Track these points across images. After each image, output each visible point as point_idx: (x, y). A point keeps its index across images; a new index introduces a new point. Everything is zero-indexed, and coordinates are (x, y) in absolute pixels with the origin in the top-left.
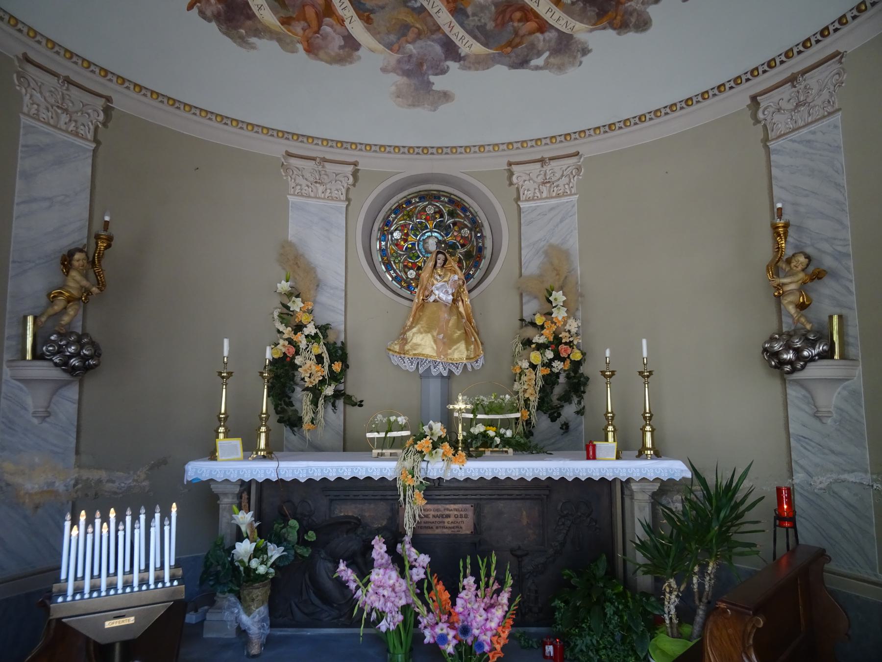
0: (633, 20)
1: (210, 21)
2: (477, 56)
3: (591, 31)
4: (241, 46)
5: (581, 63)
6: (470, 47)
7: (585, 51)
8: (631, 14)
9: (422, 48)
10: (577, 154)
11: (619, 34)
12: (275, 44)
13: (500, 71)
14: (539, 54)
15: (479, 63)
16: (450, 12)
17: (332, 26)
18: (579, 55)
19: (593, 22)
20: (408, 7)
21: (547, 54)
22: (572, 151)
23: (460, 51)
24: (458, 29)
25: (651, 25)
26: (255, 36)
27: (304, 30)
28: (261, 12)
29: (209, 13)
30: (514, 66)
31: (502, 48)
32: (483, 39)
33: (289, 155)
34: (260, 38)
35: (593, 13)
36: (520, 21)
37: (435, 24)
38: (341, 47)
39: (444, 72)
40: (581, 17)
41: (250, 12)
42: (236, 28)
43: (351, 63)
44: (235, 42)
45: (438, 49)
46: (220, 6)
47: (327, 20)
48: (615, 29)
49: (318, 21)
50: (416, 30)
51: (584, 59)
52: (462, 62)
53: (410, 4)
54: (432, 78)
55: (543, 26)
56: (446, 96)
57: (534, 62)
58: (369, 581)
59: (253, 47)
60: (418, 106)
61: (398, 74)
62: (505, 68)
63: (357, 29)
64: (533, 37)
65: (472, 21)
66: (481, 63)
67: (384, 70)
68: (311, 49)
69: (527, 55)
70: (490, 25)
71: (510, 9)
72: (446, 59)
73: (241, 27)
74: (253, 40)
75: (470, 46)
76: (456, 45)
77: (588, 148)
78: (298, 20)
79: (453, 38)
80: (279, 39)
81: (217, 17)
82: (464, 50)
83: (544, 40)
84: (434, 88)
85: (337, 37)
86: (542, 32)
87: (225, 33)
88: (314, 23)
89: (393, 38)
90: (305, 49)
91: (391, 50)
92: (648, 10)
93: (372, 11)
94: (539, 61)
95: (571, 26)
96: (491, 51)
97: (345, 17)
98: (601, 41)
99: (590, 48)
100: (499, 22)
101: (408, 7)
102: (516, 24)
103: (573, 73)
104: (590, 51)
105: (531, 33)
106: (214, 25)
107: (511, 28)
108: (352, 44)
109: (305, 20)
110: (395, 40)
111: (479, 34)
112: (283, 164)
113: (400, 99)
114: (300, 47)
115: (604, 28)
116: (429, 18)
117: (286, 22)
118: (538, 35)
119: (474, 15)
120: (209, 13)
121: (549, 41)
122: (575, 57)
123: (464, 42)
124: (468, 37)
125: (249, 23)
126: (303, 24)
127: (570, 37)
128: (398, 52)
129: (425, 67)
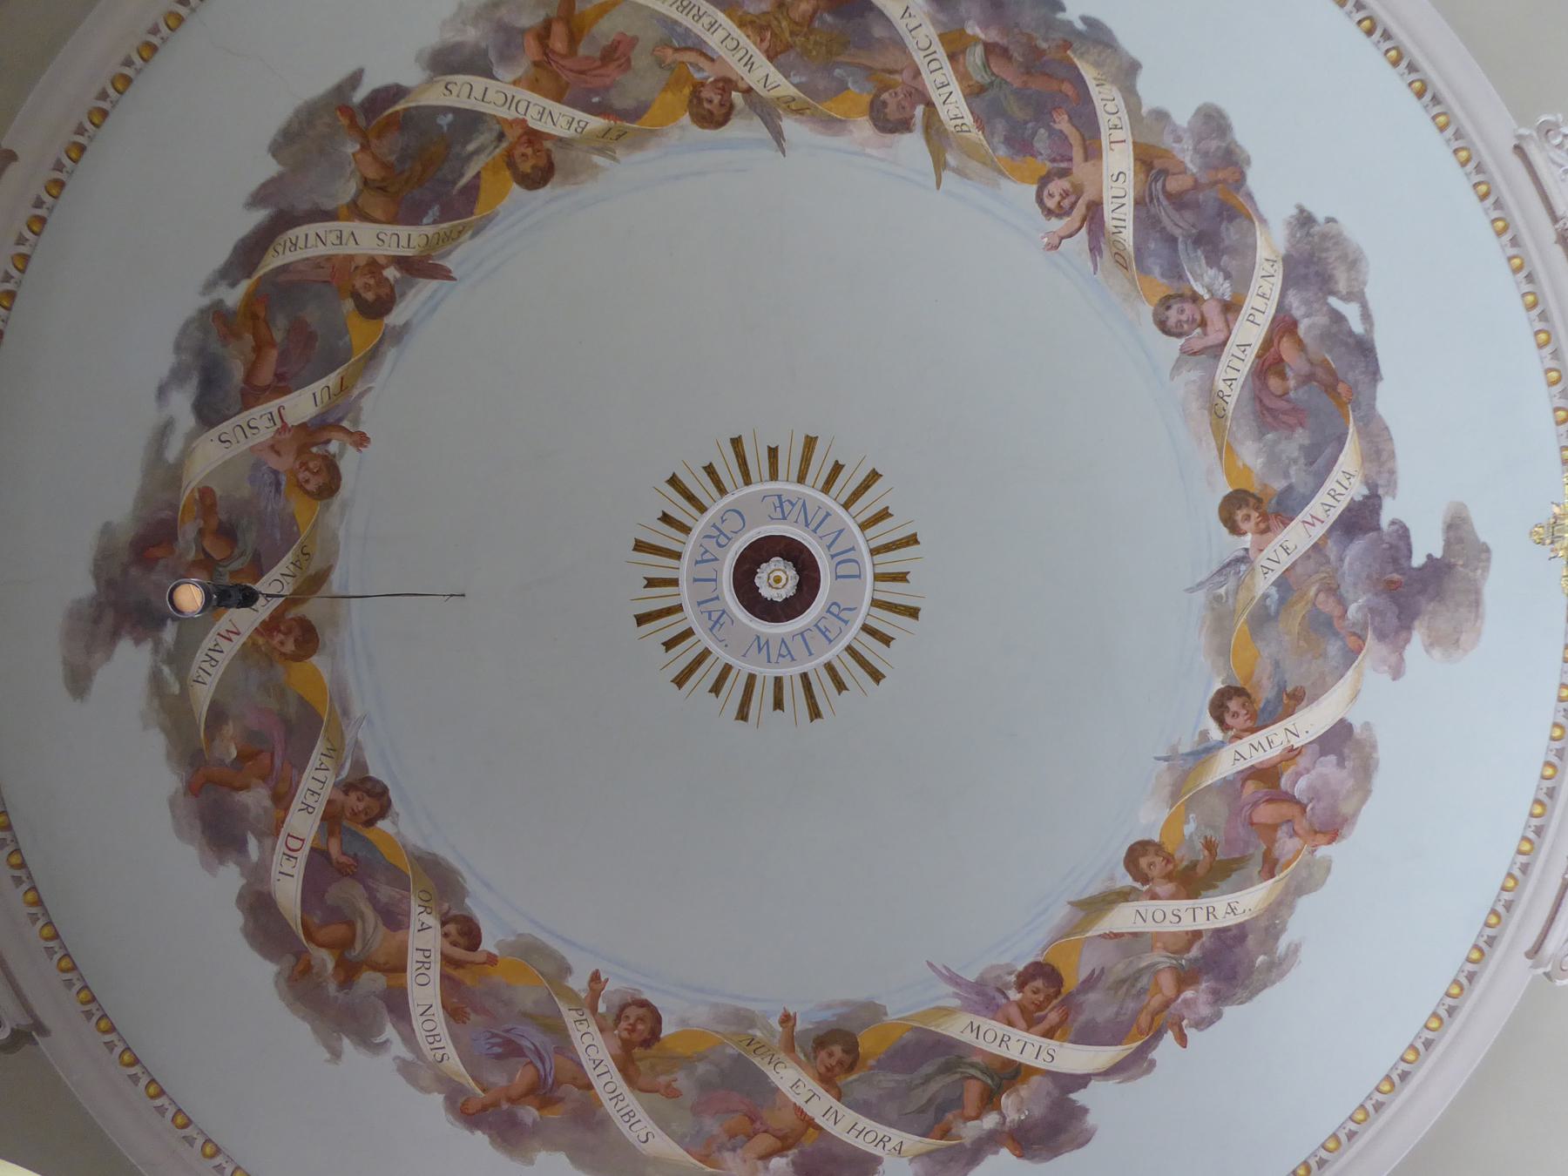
0: (1213, 144)
1: (1219, 1015)
2: (1365, 458)
3: (1263, 221)
4: (1282, 975)
5: (1330, 220)
6: (1349, 476)
7: (1304, 220)
8: (1206, 154)
9: (1355, 585)
10: (1518, 149)
11: (1248, 162)
12: (1304, 904)
13: (1389, 400)
14: (1338, 318)
15: (1378, 452)
16: (1285, 525)
17: (1299, 775)
18: (1316, 229)
19: (1245, 223)
20: (1277, 613)
21: (1334, 302)
22: (1515, 163)
23: (1358, 498)
24: (1315, 507)
25: (1205, 105)
26: (1277, 938)
27: (1294, 834)
28: (1240, 911)
29: (1205, 1010)
30: (1374, 374)
31: (1342, 405)
32: (1328, 451)
33: (1535, 951)
34: (1283, 930)
35: (1232, 230)
36: (1283, 376)
37: (1306, 556)
38: (1341, 763)
39: (1403, 533)
40: (1247, 250)
41: (1234, 932)
42: (1251, 969)
43: (1374, 747)
44: (1273, 983)
45: (1358, 546)
46: (1204, 985)
47: (1284, 782)
48: (1243, 176)
49: (1283, 801)
50: (1322, 597)
51: (1320, 216)
52: (1381, 492)
53: (1273, 609)
54: (1418, 560)
55: (1284, 326)
56: (1457, 528)
57: (1357, 327)
58: (1010, 1024)
59: (1295, 950)
60: (1478, 592)
61: (1407, 641)
62: (1382, 390)
63: (1310, 722)
64: (1307, 340)
65: (1297, 475)
66: (1378, 451)
67: (1397, 672)
68: (1332, 830)
69: (1346, 344)
70: (1301, 437)
71: (1267, 402)
72: (1378, 528)
73: (1253, 962)
74: (1283, 944)
75: (1345, 482)
76: (1348, 509)
77: (1496, 127)
78: (1274, 841)
79: (1335, 514)
80: (1298, 889)
81: (1220, 998)
82: (1358, 491)
83: (1308, 315)
84: (1438, 554)
85: (1319, 769)
86: (1295, 324)
87: (1250, 998)
88: (1286, 809)
89: (1333, 648)
90: (1329, 843)
91: (1360, 650)
92: (1185, 125)
93: (1281, 689)
94: (1351, 311)
95: (1267, 265)
96: (1351, 429)
97: (1286, 745)
98: (1275, 193)
99: (1294, 212)
100: (1292, 420)
101: (1277, 613)
102: (1292, 383)
103: (1354, 229)
104: (1302, 210)
105: (1300, 345)
106: (1229, 1011)
107: (1301, 391)
108: (1339, 739)
109: (1274, 827)
110: (1339, 643)
111: (1321, 461)
112: (1547, 974)
113: (1464, 637)
114: (1323, 851)
115: (1250, 196)
116: (1299, 570)
117: (1270, 867)
118: (1302, 330)
119: (1286, 475)
120: (1205, 1010)
121: (1307, 302)
122: (1325, 236)
123: (1340, 489)
124: (1330, 484)
125: (1251, 941)
126: (1282, 833)
127: (1288, 261)
128: (1361, 638)
129: (1396, 576)
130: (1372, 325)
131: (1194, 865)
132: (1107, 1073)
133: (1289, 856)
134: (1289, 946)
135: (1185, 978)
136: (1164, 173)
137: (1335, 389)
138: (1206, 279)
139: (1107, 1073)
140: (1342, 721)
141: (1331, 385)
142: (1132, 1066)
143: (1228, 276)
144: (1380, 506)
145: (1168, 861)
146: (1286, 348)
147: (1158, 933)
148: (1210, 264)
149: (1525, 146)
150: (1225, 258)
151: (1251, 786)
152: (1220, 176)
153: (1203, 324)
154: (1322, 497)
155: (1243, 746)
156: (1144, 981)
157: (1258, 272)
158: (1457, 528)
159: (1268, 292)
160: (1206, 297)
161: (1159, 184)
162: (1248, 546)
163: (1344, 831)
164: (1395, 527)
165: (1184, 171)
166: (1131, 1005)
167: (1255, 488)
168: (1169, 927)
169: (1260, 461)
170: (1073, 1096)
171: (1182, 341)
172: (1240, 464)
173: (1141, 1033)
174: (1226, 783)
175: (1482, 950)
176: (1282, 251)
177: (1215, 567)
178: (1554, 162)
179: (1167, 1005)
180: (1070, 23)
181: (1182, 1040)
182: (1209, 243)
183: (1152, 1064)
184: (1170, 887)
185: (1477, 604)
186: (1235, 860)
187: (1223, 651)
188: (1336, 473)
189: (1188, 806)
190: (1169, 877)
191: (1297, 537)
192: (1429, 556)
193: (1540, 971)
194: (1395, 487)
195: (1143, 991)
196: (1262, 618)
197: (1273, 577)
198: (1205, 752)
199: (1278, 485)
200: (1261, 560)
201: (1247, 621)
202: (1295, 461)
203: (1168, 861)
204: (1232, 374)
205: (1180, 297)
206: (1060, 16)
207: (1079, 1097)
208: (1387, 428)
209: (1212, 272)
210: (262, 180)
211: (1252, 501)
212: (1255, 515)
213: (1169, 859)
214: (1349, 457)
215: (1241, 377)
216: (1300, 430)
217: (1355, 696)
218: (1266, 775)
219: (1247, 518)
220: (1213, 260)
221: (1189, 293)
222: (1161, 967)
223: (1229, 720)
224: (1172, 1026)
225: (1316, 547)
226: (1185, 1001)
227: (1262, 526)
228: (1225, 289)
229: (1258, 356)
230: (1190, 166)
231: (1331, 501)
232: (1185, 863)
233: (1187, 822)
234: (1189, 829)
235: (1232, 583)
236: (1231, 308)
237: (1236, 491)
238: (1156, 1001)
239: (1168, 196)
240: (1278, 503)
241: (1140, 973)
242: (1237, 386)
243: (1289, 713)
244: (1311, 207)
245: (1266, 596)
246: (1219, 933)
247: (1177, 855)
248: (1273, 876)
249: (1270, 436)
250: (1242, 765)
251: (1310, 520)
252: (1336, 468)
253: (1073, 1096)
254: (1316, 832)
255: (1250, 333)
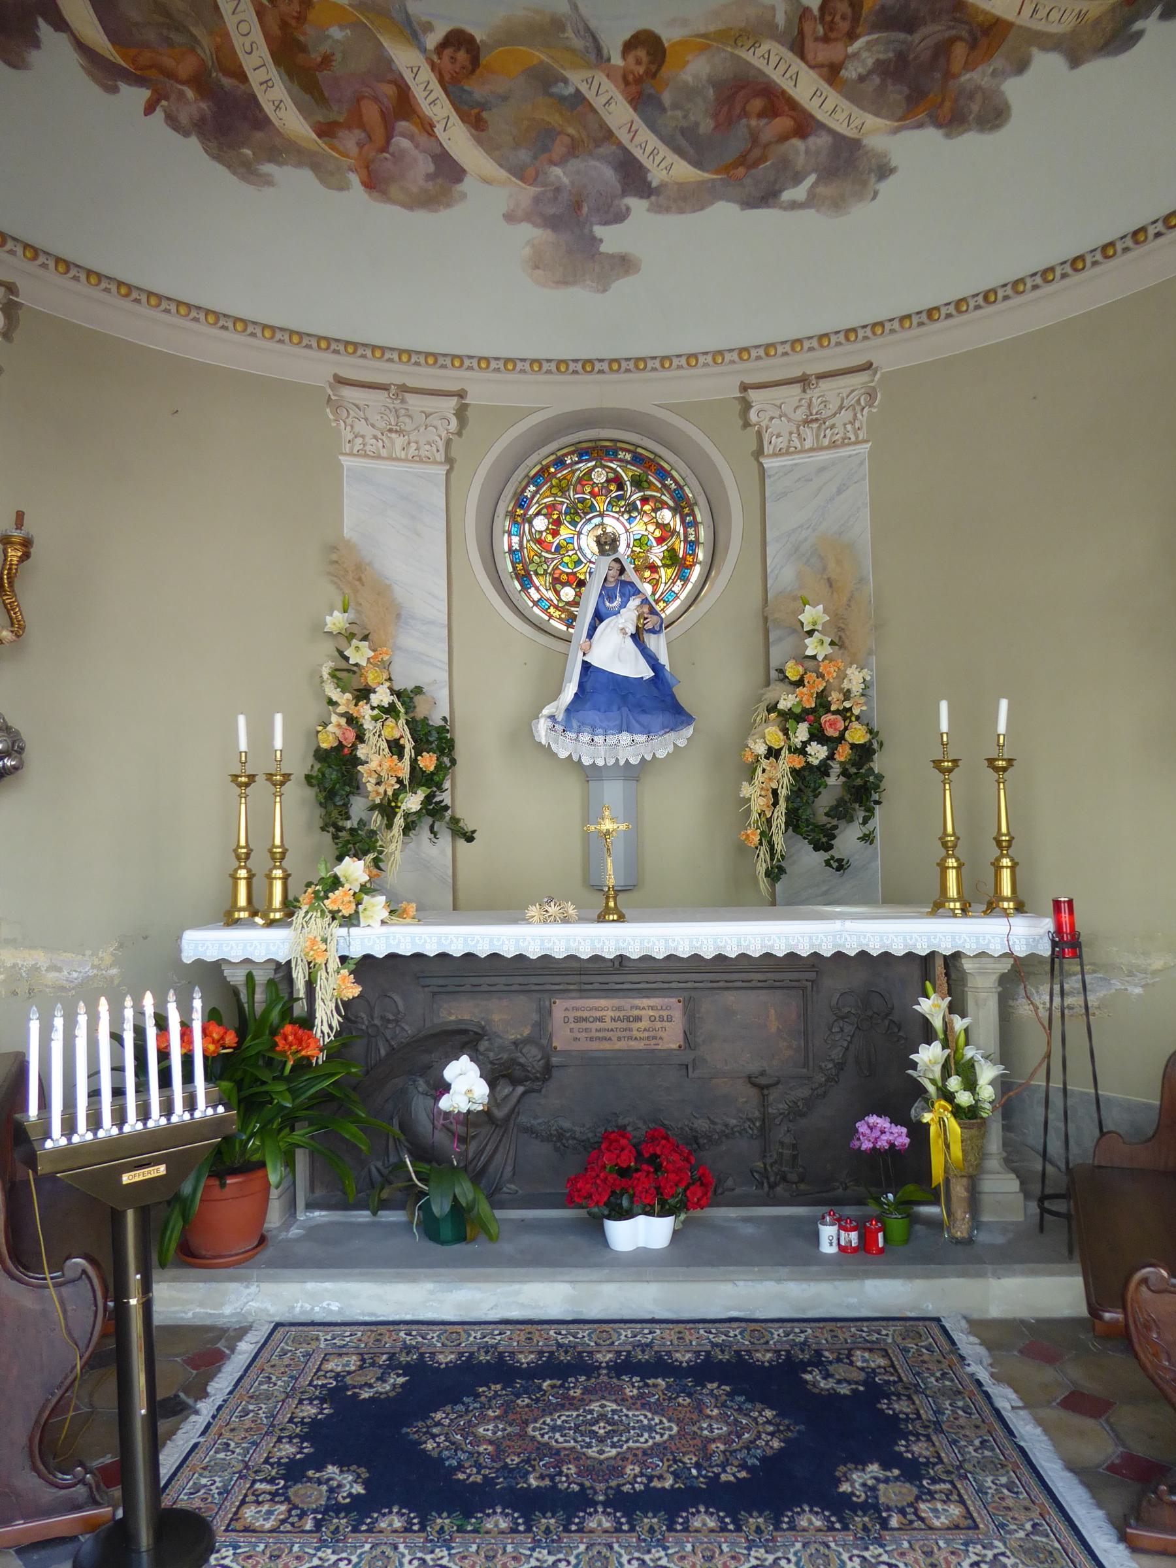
0: (975, 108)
1: (186, 134)
2: (681, 186)
3: (896, 131)
4: (243, 178)
5: (876, 194)
7: (884, 171)
8: (971, 97)
10: (868, 366)
11: (948, 136)
12: (306, 176)
13: (725, 212)
14: (797, 179)
16: (630, 102)
17: (411, 138)
18: (873, 179)
20: (551, 95)
21: (812, 178)
23: (650, 177)
24: (645, 134)
25: (1008, 117)
26: (270, 161)
27: (360, 145)
31: (727, 169)
33: (341, 381)
34: (280, 164)
36: (761, 115)
38: (429, 177)
39: (619, 217)
43: (448, 205)
44: (235, 173)
46: (203, 105)
47: (403, 125)
48: (939, 126)
49: (386, 128)
52: (653, 198)
53: (555, 90)
54: (599, 231)
55: (804, 125)
56: (624, 264)
57: (787, 195)
59: (267, 181)
60: (575, 283)
61: (535, 225)
63: (457, 140)
64: (787, 144)
66: (688, 199)
67: (509, 217)
68: (374, 183)
70: (706, 125)
72: (625, 193)
74: (268, 168)
75: (667, 166)
76: (641, 166)
77: (890, 355)
78: (349, 128)
79: (637, 153)
80: (316, 164)
82: (657, 176)
83: (807, 152)
84: (603, 248)
85: (421, 157)
88: (379, 133)
93: (483, 106)
94: (797, 193)
95: (858, 123)
96: (707, 176)
97: (435, 119)
99: (893, 164)
101: (551, 95)
104: (892, 171)
105: (783, 138)
106: (194, 142)
108: (449, 171)
109: (362, 126)
111: (683, 143)
114: (354, 179)
115: (920, 126)
117: (326, 131)
119: (676, 106)
120: (184, 118)
122: (865, 184)
123: (658, 159)
124: (664, 150)
125: (259, 135)
126: (358, 134)
128: (533, 182)
129: (585, 210)
130: (785, 209)
131: (303, 48)
132: (81, 47)
133: (341, 148)
134: (269, 175)
135: (201, 82)
136: (973, 45)
137: (742, 164)
138: (865, 54)
139: (81, 47)
140: (464, 171)
141: (743, 161)
142: (106, 73)
143: (862, 79)
144: (641, 197)
145: (298, 19)
146: (784, 123)
147: (227, 34)
148: (879, 63)
149: (869, 372)
150: (877, 80)
151: (389, 90)
152: (947, 104)
153: (826, 39)
154: (653, 141)
155: (426, 74)
156: (179, 38)
157: (856, 111)
158: (624, 264)
159: (836, 116)
160: (850, 50)
161: (964, 34)
162: (613, 61)
163: (375, 194)
164: (624, 208)
165: (969, 66)
166: (151, 35)
167: (665, 72)
168: (238, 42)
169: (690, 79)
170: (41, 22)
171: (816, 12)
172: (689, 58)
173: (134, 61)
174: (388, 62)
175: (327, 343)
176: (865, 142)
177: (593, 24)
178: (853, 391)
179: (171, 75)
180: (1146, 16)
181: (149, 109)
182: (895, 69)
183: (114, 90)
184: (276, 31)
185: (564, 282)
186: (321, 93)
187: (511, 36)
188: (672, 157)
189: (357, 25)
190: (284, 25)
191: (619, 114)
192: (601, 241)
193: (330, 392)
194: (656, 212)
195: (170, 43)
196: (544, 80)
197: (583, 88)
198: (412, 32)
199: (667, 98)
200: (600, 77)
201: (542, 62)
202: (685, 117)
203: (298, 19)
204: (774, 60)
205: (856, 20)
206: (1158, 11)
207: (45, 30)
208: (702, 209)
209: (870, 62)
210: (1140, 42)
211: (653, 68)
212: (641, 70)
213: (301, 18)
214: (682, 171)
215: (769, 71)
216: (712, 126)
217: (486, 181)
218: (403, 105)
219: (638, 62)
220: (881, 68)
221: (858, 31)
222: (199, 51)
223: (448, 52)
224: (155, 91)
225: (609, 135)
226: (182, 94)
227: (630, 78)
228: (850, 72)
229: (784, 92)
230: (968, 76)
231: (649, 149)
232: (302, 38)
233: (342, 28)
234: (336, 33)
235: (578, 43)
236: (832, 73)
237: (664, 51)
238: (168, 62)
239: (952, 41)
240: (650, 95)
241: (180, 28)
242: (759, 63)
243: (463, 117)
244: (892, 179)
245: (565, 81)
246: (253, 98)
247: (307, 28)
248: (320, 136)
249: (711, 91)
250: (408, 76)
251: (634, 128)
252: (676, 157)
253: (41, 22)
254: (367, 167)
255: (805, 87)
